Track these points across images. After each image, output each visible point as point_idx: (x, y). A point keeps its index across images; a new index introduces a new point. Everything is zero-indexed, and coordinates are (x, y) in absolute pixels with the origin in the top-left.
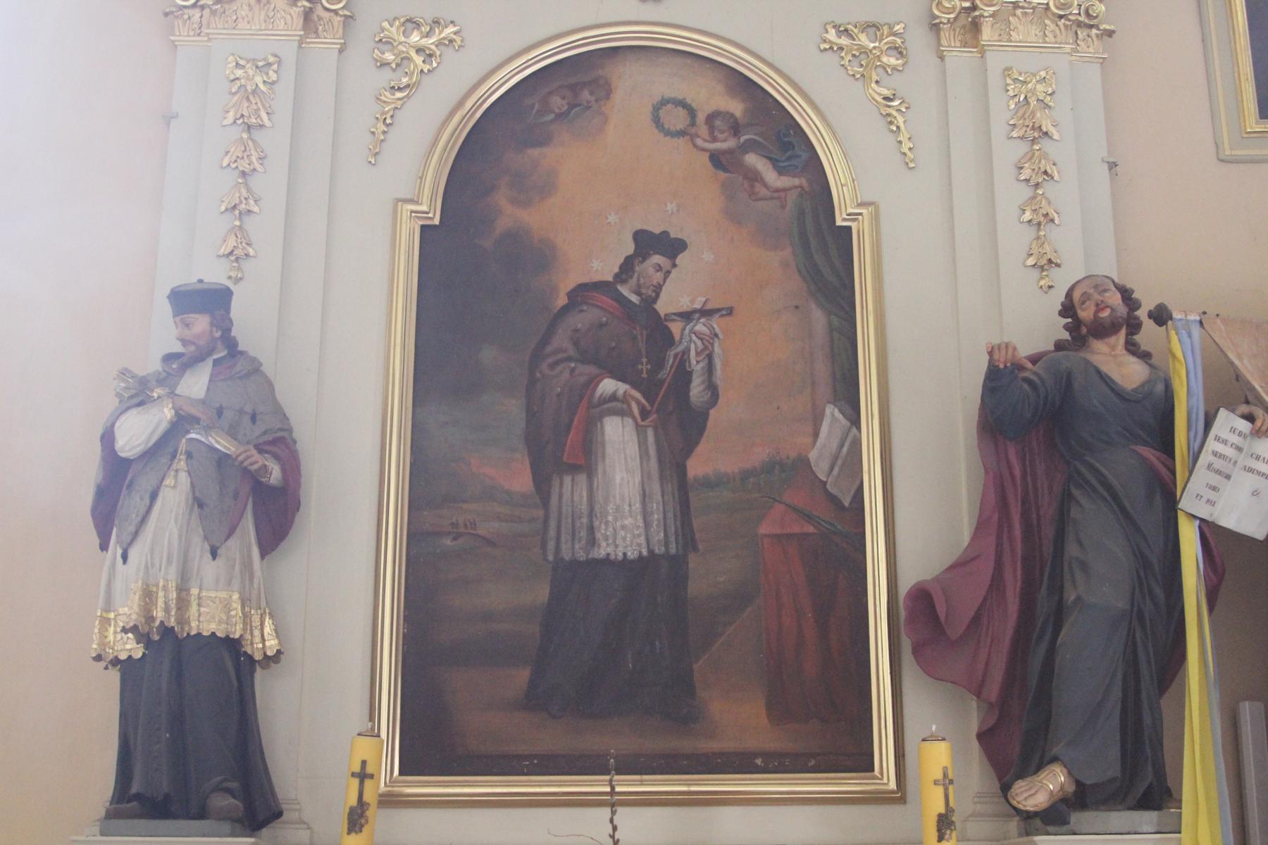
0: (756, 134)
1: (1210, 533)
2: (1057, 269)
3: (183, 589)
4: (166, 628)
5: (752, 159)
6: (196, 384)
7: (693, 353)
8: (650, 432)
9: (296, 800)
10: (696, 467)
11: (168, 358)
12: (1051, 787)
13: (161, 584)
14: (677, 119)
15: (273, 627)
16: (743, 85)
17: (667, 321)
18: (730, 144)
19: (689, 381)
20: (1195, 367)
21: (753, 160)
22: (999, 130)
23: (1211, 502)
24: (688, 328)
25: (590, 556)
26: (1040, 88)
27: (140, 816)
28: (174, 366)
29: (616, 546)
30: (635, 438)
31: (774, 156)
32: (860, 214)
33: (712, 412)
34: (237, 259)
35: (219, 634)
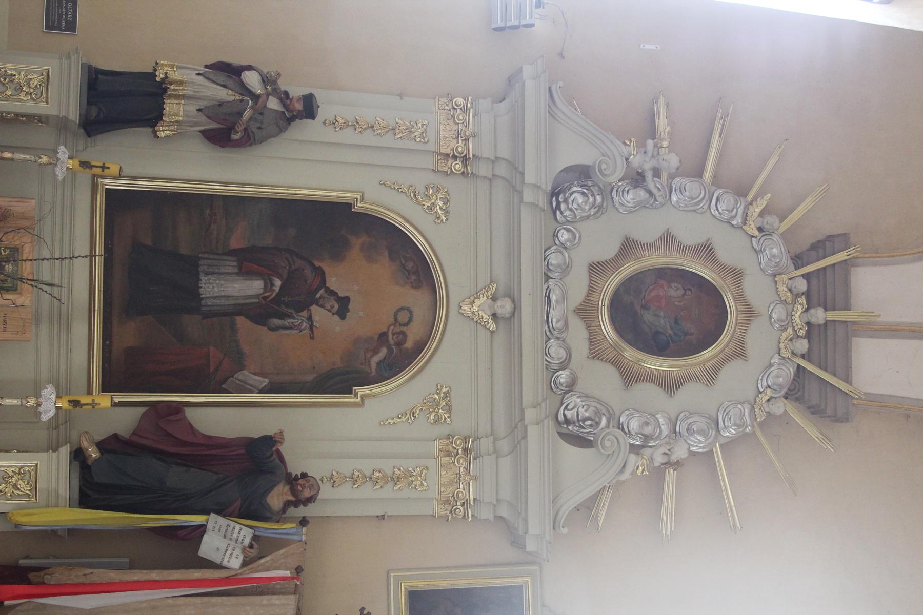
0: (396, 353)
1: (201, 530)
2: (332, 486)
3: (183, 97)
4: (167, 90)
5: (384, 351)
6: (273, 104)
9: (96, 145)
10: (241, 320)
11: (286, 94)
12: (90, 450)
13: (185, 88)
14: (403, 317)
15: (169, 135)
16: (420, 348)
17: (308, 311)
18: (391, 342)
19: (279, 318)
21: (384, 351)
24: (305, 319)
25: (200, 272)
26: (418, 483)
28: (282, 96)
29: (205, 284)
30: (254, 294)
31: (385, 361)
32: (357, 398)
34: (334, 123)
35: (164, 111)
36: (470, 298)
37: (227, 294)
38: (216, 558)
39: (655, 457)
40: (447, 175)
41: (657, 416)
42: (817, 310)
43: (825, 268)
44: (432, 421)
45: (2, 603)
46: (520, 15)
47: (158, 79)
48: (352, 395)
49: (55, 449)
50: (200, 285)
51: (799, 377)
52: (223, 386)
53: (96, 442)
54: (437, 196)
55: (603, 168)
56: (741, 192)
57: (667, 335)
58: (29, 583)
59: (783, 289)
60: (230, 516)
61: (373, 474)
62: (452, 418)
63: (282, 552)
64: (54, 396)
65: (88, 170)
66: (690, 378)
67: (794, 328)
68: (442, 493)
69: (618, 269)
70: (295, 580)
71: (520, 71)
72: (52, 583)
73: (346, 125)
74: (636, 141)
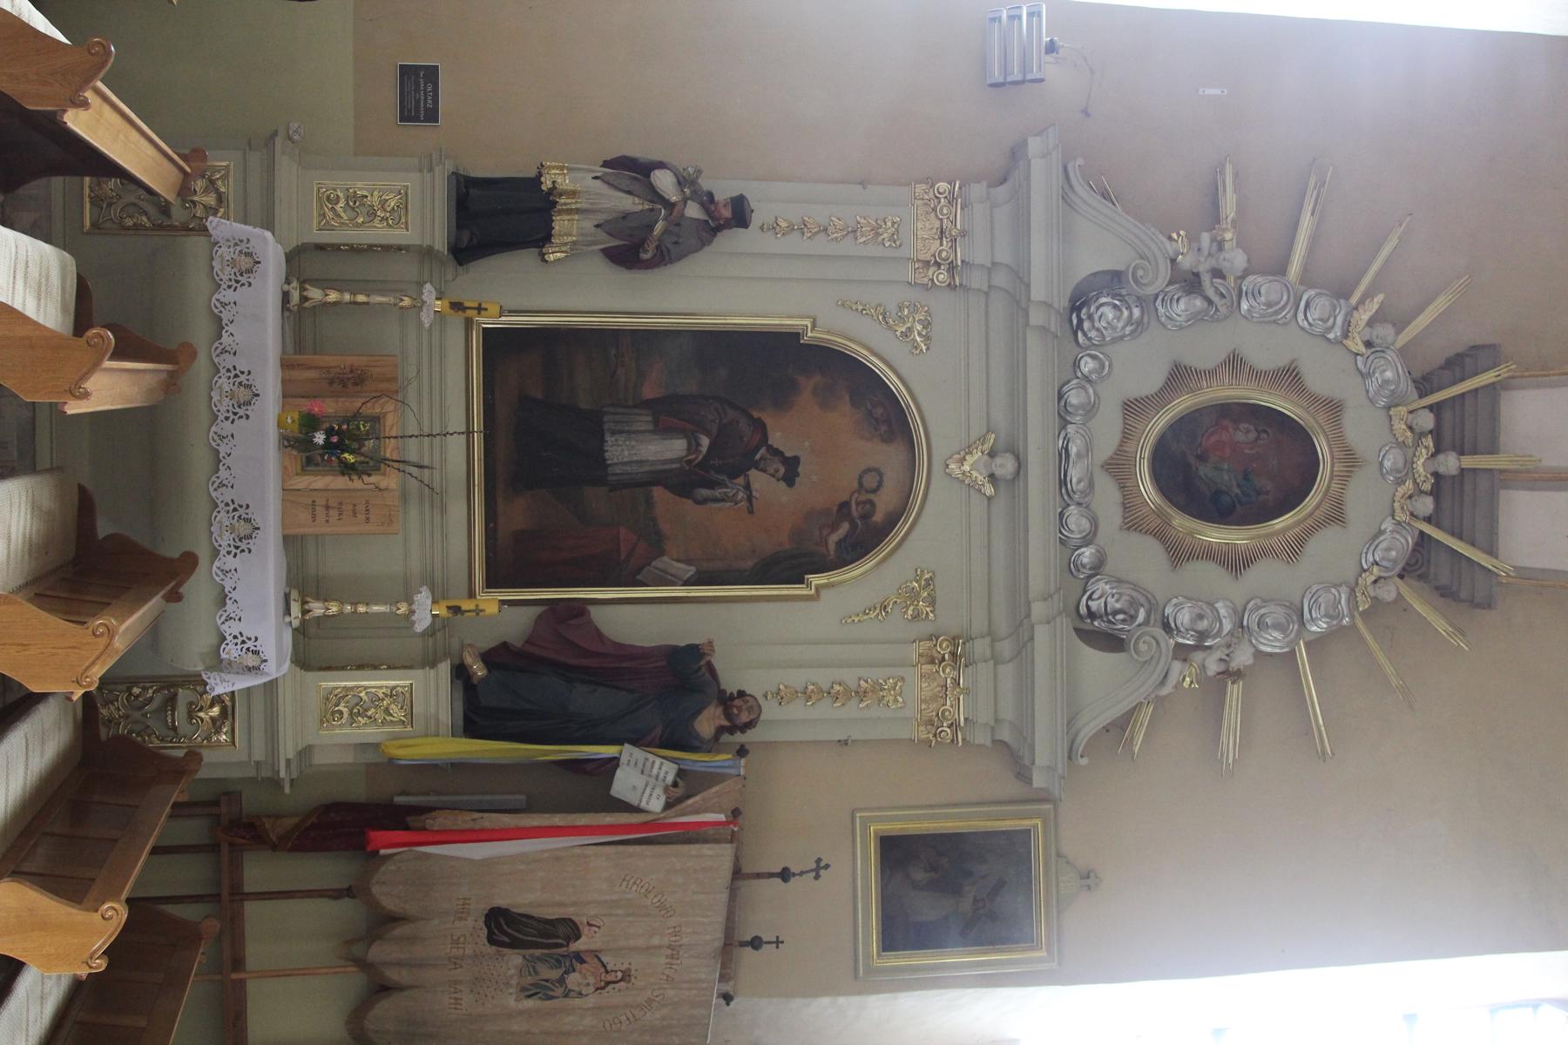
1: (614, 763)
2: (777, 704)
5: (845, 527)
6: (693, 211)
7: (725, 490)
8: (677, 465)
10: (658, 493)
11: (710, 195)
14: (870, 481)
16: (892, 521)
20: (712, 767)
21: (845, 527)
22: (862, 672)
23: (628, 764)
26: (891, 698)
27: (458, 194)
33: (690, 501)
34: (774, 228)
36: (959, 454)
37: (639, 458)
38: (632, 799)
39: (1207, 663)
40: (927, 290)
41: (1217, 605)
42: (1447, 456)
43: (1463, 395)
44: (910, 618)
45: (378, 852)
46: (1025, 68)
47: (544, 187)
48: (804, 586)
49: (433, 664)
50: (606, 448)
51: (1423, 547)
52: (638, 577)
53: (482, 651)
54: (914, 318)
55: (1138, 275)
56: (1342, 292)
57: (1233, 495)
58: (407, 828)
59: (1400, 427)
60: (648, 746)
61: (832, 687)
62: (936, 612)
63: (714, 790)
64: (429, 602)
65: (460, 313)
66: (1265, 553)
67: (1415, 481)
68: (923, 712)
69: (1167, 406)
70: (731, 826)
71: (1024, 143)
72: (435, 828)
73: (791, 228)
74: (1186, 235)
